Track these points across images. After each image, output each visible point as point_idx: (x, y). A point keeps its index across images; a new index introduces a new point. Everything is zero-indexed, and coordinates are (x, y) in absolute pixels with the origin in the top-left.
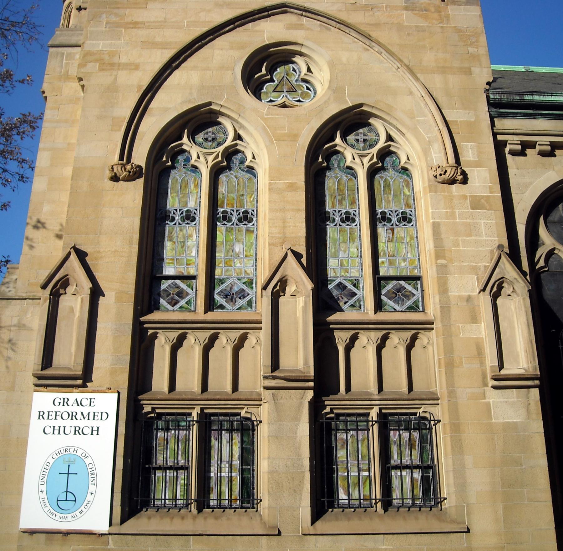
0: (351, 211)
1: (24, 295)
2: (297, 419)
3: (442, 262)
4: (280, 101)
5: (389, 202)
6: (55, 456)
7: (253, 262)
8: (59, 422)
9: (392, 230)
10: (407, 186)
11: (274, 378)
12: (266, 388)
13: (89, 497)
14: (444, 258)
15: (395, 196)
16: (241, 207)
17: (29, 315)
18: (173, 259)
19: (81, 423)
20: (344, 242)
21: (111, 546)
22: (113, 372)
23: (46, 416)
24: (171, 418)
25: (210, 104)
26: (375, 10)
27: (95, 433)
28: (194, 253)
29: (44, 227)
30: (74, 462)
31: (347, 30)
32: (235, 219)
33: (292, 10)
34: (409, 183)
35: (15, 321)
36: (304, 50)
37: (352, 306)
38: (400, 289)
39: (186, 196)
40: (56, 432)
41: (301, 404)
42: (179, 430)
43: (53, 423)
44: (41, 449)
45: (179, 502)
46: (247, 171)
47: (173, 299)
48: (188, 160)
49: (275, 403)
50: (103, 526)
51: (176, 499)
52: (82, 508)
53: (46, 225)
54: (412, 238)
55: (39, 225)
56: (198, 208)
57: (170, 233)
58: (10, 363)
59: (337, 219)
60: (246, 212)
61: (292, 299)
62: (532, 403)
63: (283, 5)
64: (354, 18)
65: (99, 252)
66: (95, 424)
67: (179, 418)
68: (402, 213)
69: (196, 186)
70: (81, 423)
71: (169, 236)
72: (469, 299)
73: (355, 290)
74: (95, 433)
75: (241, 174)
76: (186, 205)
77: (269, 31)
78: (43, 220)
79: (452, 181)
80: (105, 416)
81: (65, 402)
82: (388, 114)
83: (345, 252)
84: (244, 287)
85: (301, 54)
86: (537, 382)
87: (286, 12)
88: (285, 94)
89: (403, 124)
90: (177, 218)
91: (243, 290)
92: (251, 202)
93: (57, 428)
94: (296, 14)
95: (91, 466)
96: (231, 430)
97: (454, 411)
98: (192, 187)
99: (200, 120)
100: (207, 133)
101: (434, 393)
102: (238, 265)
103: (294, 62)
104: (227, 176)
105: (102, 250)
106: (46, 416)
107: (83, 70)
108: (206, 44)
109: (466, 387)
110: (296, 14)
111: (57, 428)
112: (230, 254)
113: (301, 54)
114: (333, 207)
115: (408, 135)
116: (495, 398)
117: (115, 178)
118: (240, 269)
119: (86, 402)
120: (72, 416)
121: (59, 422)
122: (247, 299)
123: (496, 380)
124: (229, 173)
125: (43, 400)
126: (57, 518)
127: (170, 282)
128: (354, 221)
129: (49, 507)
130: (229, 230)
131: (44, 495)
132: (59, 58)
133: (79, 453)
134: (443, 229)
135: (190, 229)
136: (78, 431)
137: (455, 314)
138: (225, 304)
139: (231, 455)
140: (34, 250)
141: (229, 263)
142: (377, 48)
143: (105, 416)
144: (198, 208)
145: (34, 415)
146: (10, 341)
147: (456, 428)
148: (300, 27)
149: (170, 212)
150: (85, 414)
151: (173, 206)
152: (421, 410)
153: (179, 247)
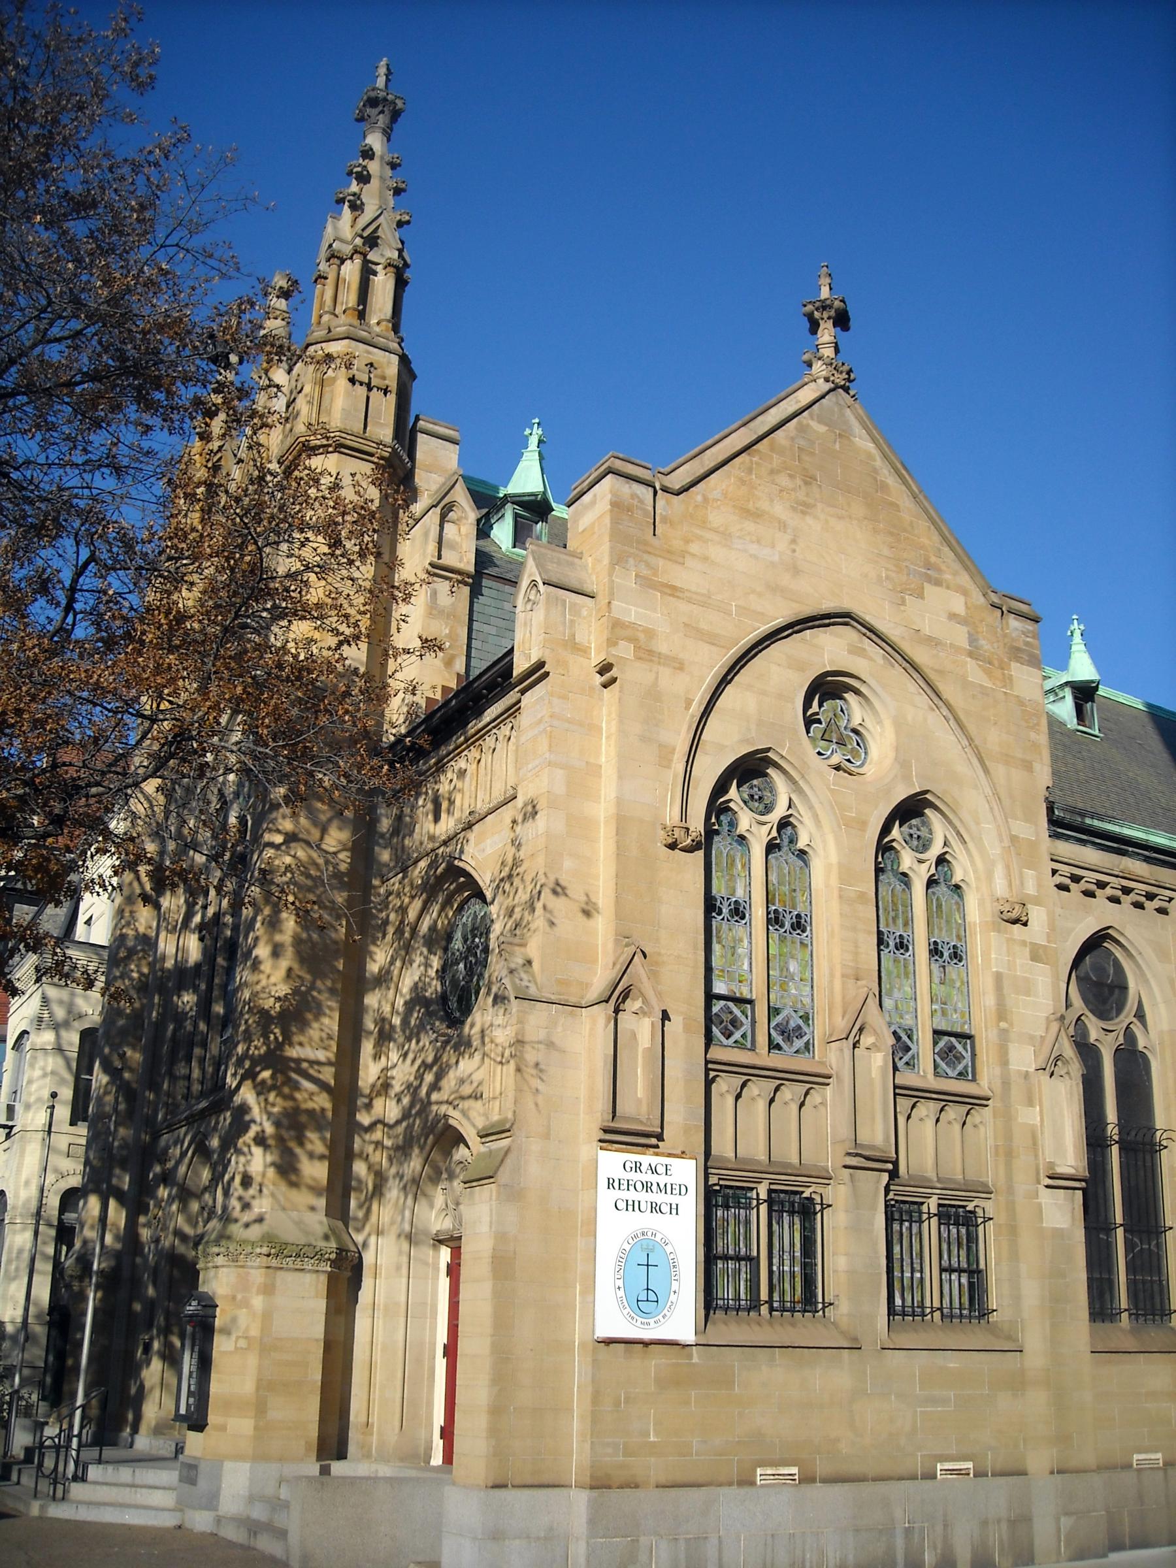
0: (905, 935)
1: (553, 998)
2: (874, 1208)
3: (1003, 1025)
4: (836, 759)
5: (941, 930)
6: (631, 1241)
7: (808, 989)
8: (632, 1195)
9: (944, 967)
10: (958, 910)
11: (857, 1155)
13: (673, 1297)
14: (1005, 1020)
15: (948, 922)
16: (794, 908)
17: (560, 1029)
18: (723, 971)
19: (659, 1198)
20: (898, 976)
21: (695, 1360)
22: (687, 1130)
23: (616, 1185)
24: (731, 1192)
25: (768, 750)
26: (939, 647)
27: (674, 1211)
28: (746, 967)
29: (566, 895)
30: (652, 1250)
31: (915, 675)
32: (787, 926)
33: (855, 624)
34: (961, 907)
35: (542, 1035)
36: (863, 689)
37: (907, 1063)
38: (951, 1048)
39: (732, 878)
40: (630, 1208)
41: (877, 1189)
42: (740, 1208)
43: (625, 1195)
44: (614, 1230)
45: (743, 1303)
46: (798, 856)
47: (726, 1028)
48: (733, 824)
49: (854, 1186)
50: (687, 1334)
51: (739, 1300)
52: (665, 1311)
53: (568, 892)
54: (962, 983)
55: (559, 889)
56: (747, 899)
57: (718, 931)
58: (540, 1099)
59: (892, 944)
60: (798, 916)
61: (866, 1053)
62: (1076, 1207)
63: (847, 615)
64: (920, 656)
65: (659, 954)
66: (674, 1199)
67: (738, 1192)
68: (954, 947)
69: (743, 866)
70: (659, 1198)
71: (718, 937)
72: (1026, 1075)
73: (909, 1043)
74: (674, 1211)
75: (793, 859)
76: (733, 894)
77: (831, 650)
78: (562, 883)
79: (1015, 921)
80: (683, 1189)
81: (637, 1167)
82: (954, 812)
83: (899, 989)
84: (800, 1022)
85: (857, 692)
86: (1084, 1184)
87: (846, 624)
88: (835, 746)
89: (968, 830)
90: (725, 911)
91: (799, 1027)
92: (804, 902)
93: (630, 1203)
94: (859, 631)
95: (672, 1256)
96: (792, 1213)
97: (1011, 1208)
98: (740, 867)
99: (750, 769)
100: (752, 788)
101: (985, 1185)
102: (793, 991)
103: (842, 698)
104: (777, 858)
105: (663, 952)
106: (616, 1185)
107: (614, 651)
108: (760, 651)
109: (1023, 1184)
110: (859, 631)
111: (630, 1203)
112: (785, 973)
113: (857, 692)
114: (887, 925)
115: (970, 845)
116: (1047, 1198)
117: (672, 846)
118: (795, 996)
119: (661, 1169)
120: (647, 1187)
121: (632, 1195)
122: (805, 1039)
123: (1050, 1177)
124: (779, 854)
125: (612, 1162)
126: (638, 1324)
127: (722, 1003)
128: (907, 950)
129: (628, 1309)
130: (782, 939)
131: (621, 1293)
132: (560, 608)
133: (658, 1238)
134: (1006, 983)
135: (739, 930)
136: (655, 1208)
137: (1016, 1093)
138: (782, 1043)
139: (792, 1245)
140: (555, 929)
141: (784, 987)
142: (945, 711)
143: (683, 1189)
144: (747, 899)
145: (602, 1183)
146: (537, 1064)
147: (1013, 1230)
148: (861, 652)
149: (716, 900)
150: (662, 1186)
151: (719, 891)
152: (974, 1204)
153: (729, 955)
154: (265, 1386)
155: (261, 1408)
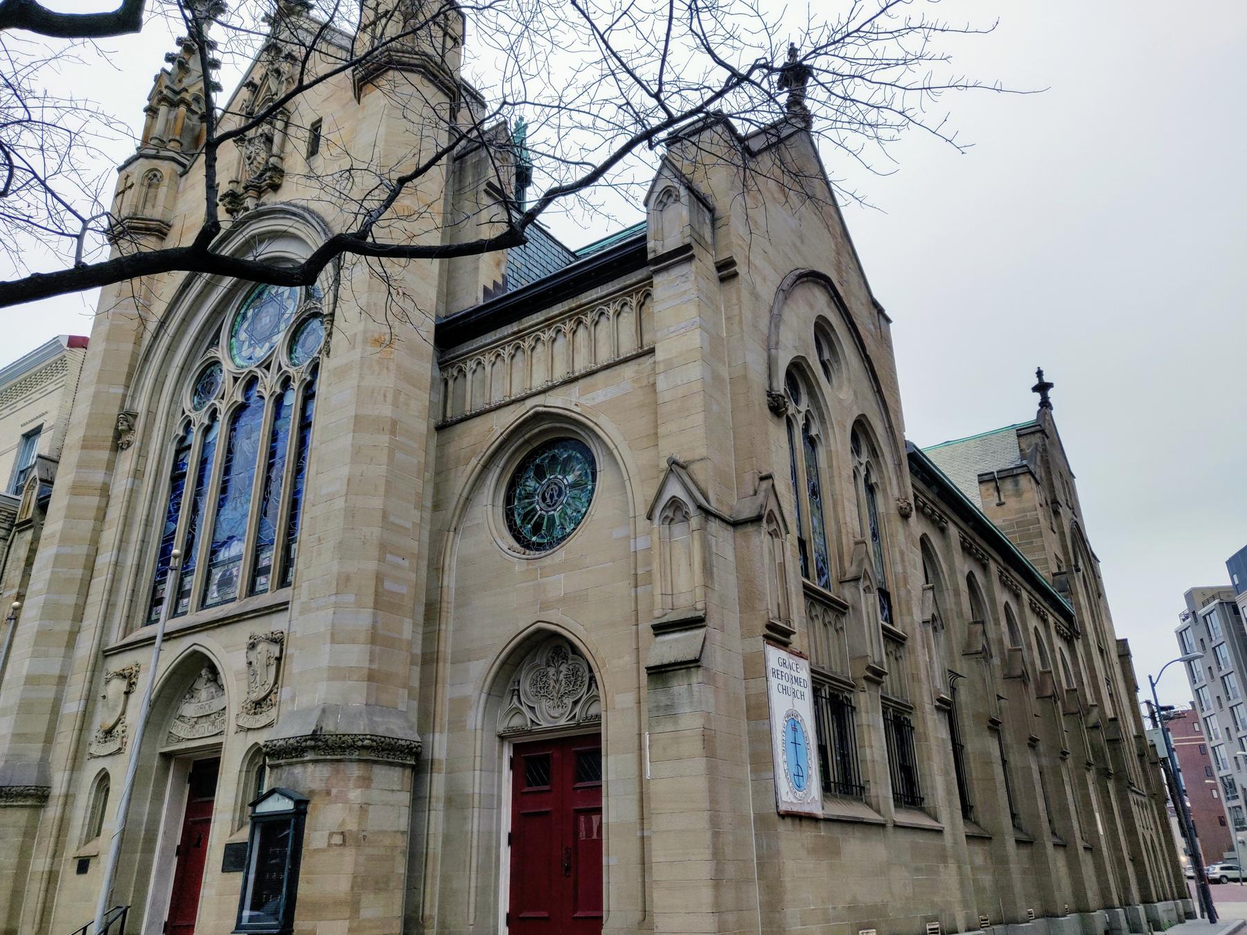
12: (866, 678)
154: (361, 883)
155: (355, 906)
